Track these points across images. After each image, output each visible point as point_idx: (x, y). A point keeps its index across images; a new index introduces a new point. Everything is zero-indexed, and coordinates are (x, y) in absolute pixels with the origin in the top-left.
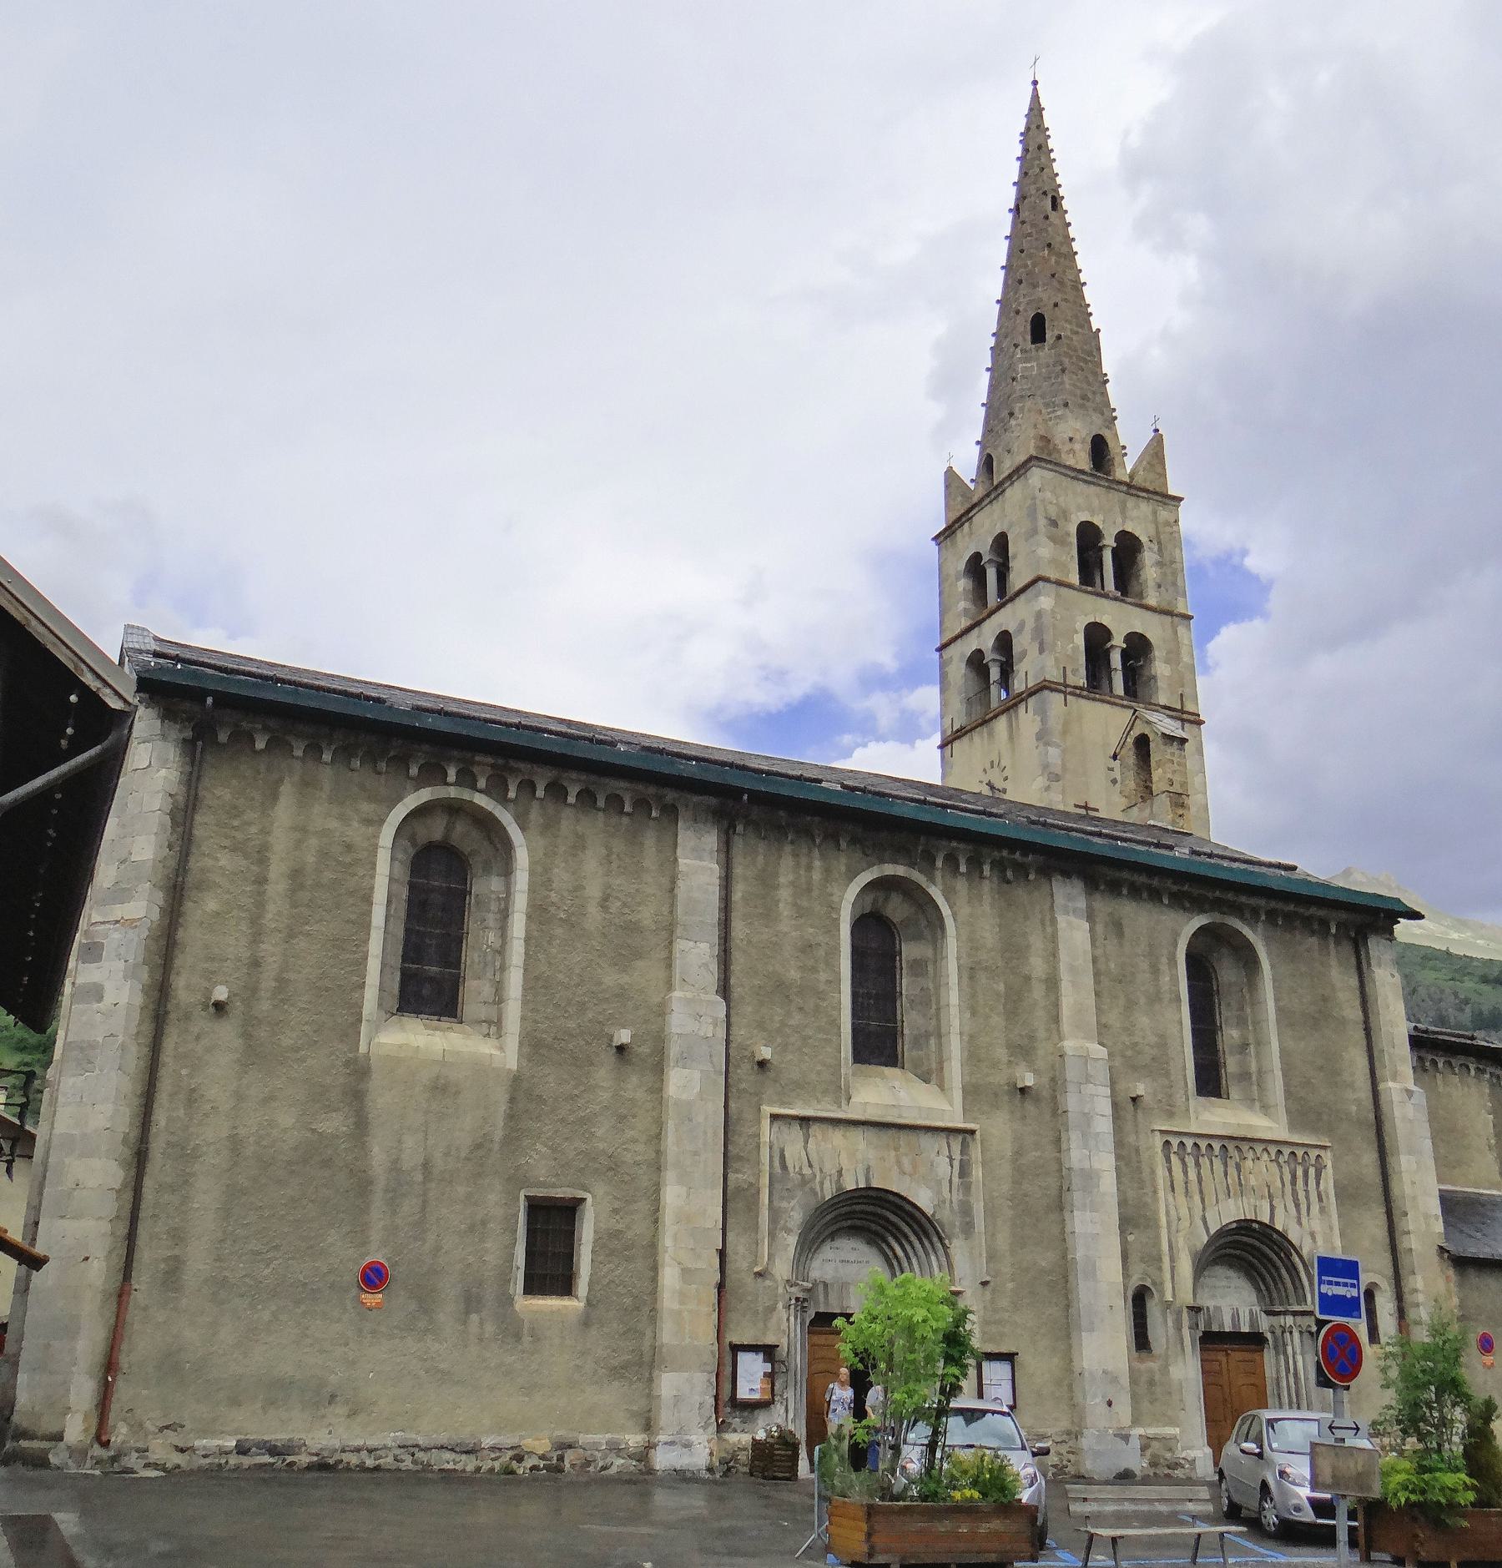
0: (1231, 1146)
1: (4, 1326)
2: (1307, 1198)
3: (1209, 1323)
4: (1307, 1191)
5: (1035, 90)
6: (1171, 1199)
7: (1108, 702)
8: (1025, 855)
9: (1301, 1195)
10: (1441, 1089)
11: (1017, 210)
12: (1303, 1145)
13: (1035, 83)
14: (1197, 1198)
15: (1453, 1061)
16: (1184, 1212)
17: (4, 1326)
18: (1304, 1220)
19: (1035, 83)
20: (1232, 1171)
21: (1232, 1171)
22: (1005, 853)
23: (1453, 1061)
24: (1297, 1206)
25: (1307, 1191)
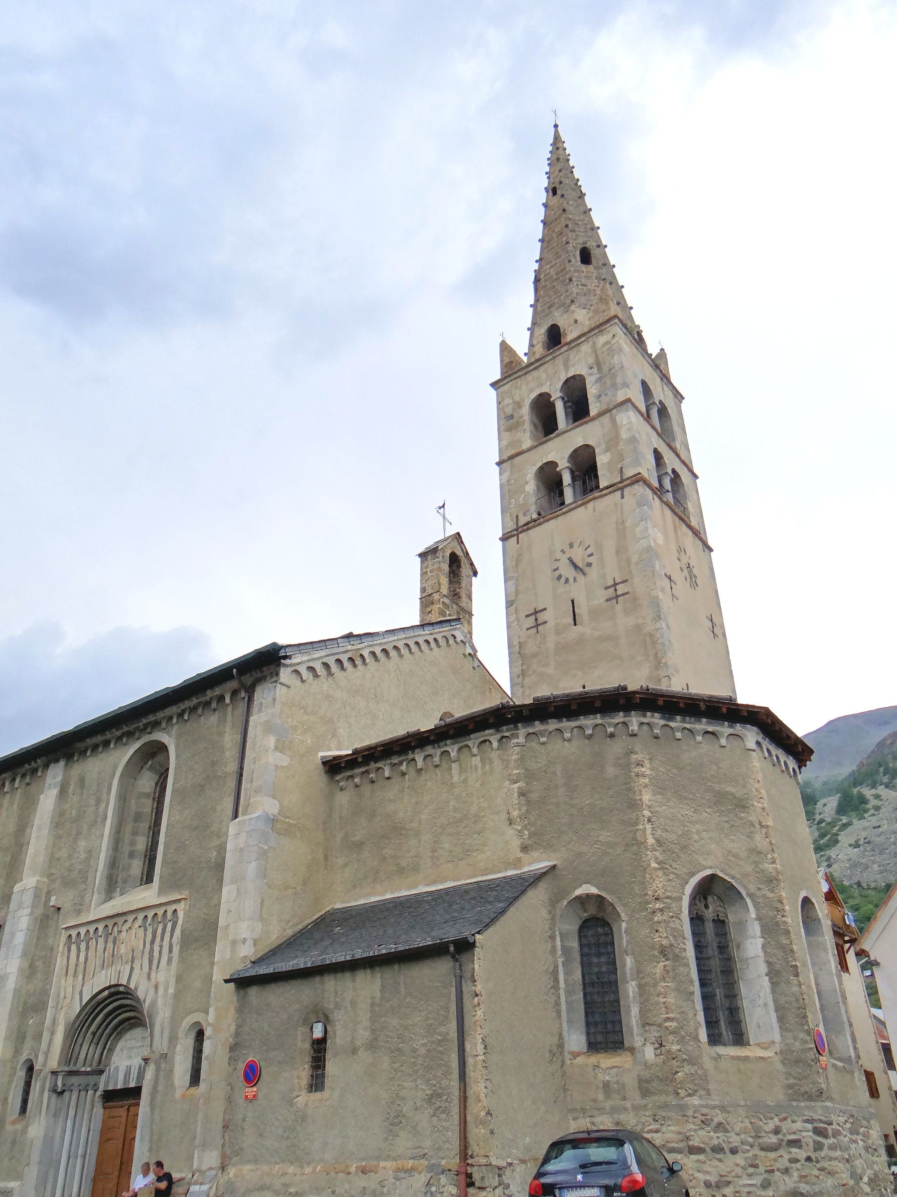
0: (110, 923)
1: (608, 1190)
2: (160, 952)
3: (107, 1083)
4: (161, 946)
5: (556, 132)
6: (63, 981)
7: (600, 497)
8: (35, 762)
9: (156, 954)
10: (456, 779)
11: (582, 195)
12: (161, 905)
13: (556, 126)
14: (80, 977)
15: (470, 743)
16: (70, 990)
17: (608, 1190)
18: (153, 975)
19: (556, 126)
20: (110, 945)
21: (110, 945)
22: (27, 766)
23: (470, 743)
24: (151, 962)
25: (161, 946)
